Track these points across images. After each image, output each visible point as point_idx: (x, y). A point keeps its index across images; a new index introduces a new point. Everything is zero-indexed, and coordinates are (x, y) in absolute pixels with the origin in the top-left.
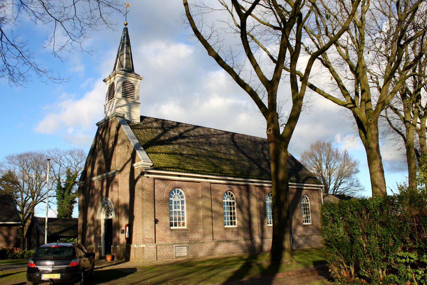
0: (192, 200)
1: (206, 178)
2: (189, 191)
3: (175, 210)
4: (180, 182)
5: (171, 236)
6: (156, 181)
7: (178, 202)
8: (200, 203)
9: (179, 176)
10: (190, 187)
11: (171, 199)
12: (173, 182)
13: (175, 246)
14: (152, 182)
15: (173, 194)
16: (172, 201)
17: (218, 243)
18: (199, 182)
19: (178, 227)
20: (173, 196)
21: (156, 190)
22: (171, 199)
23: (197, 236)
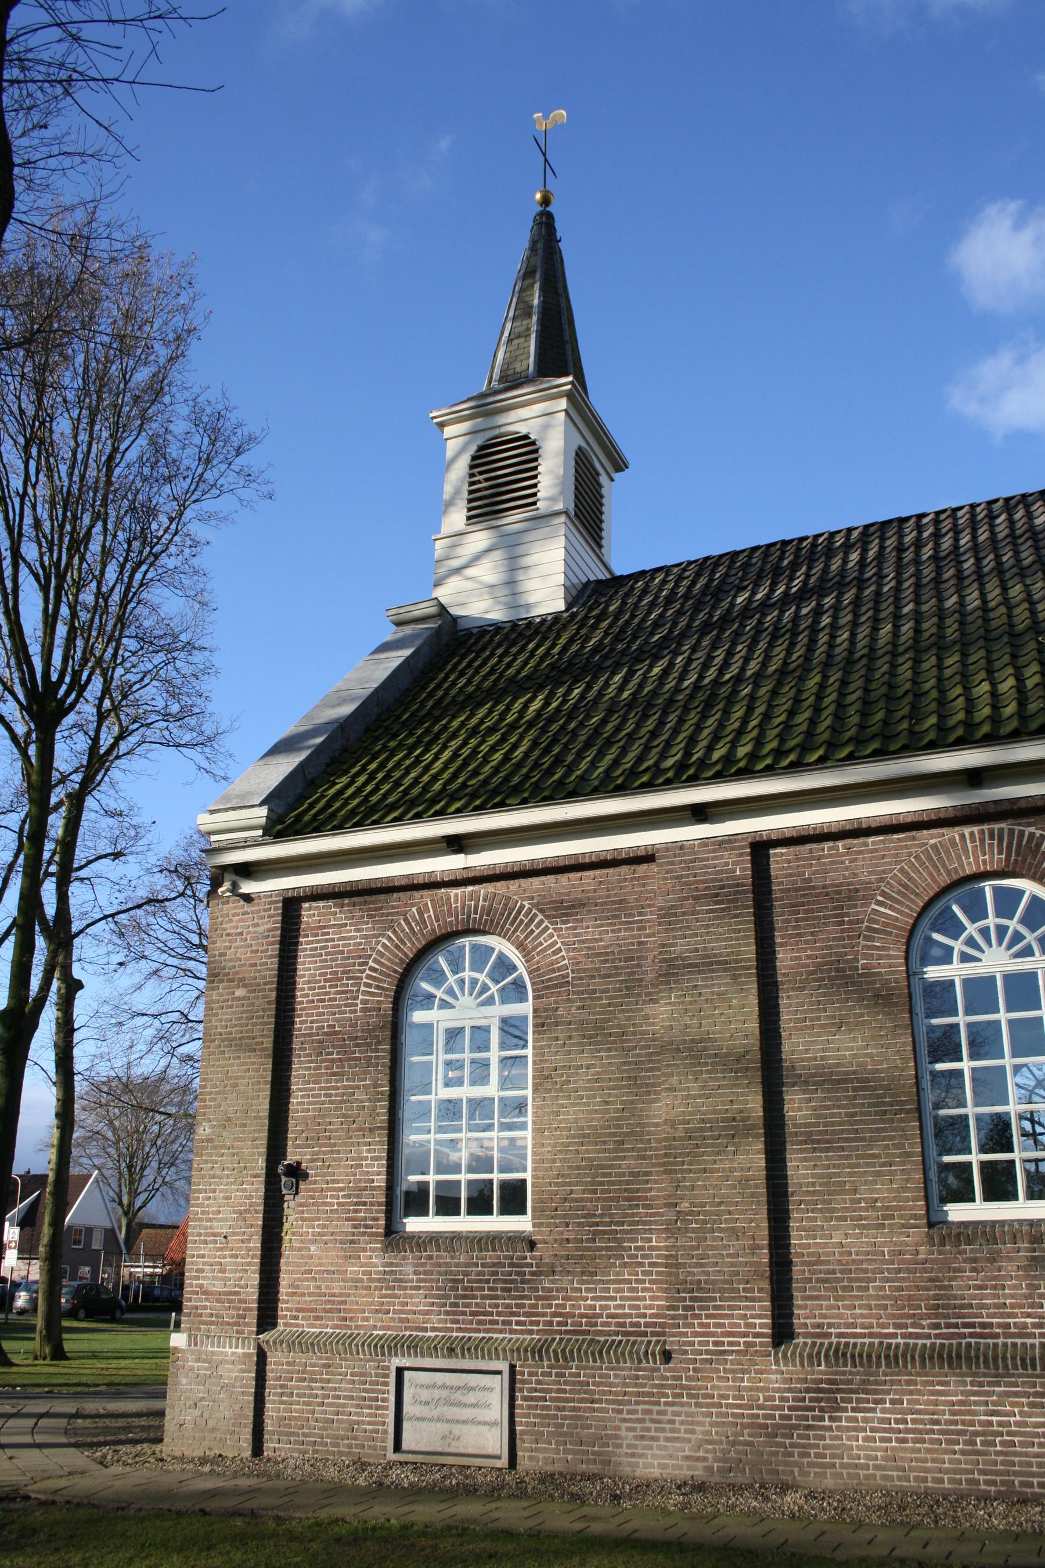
0: (582, 1014)
1: (700, 813)
2: (555, 940)
3: (453, 1093)
4: (483, 890)
5: (391, 1282)
6: (310, 913)
7: (481, 1032)
8: (663, 1014)
9: (456, 844)
10: (562, 910)
11: (934, 972)
12: (426, 897)
13: (397, 1362)
14: (270, 923)
15: (955, 929)
16: (429, 1026)
17: (857, 1369)
18: (647, 857)
19: (1022, 1209)
20: (958, 946)
21: (307, 968)
22: (934, 972)
23: (629, 1296)
